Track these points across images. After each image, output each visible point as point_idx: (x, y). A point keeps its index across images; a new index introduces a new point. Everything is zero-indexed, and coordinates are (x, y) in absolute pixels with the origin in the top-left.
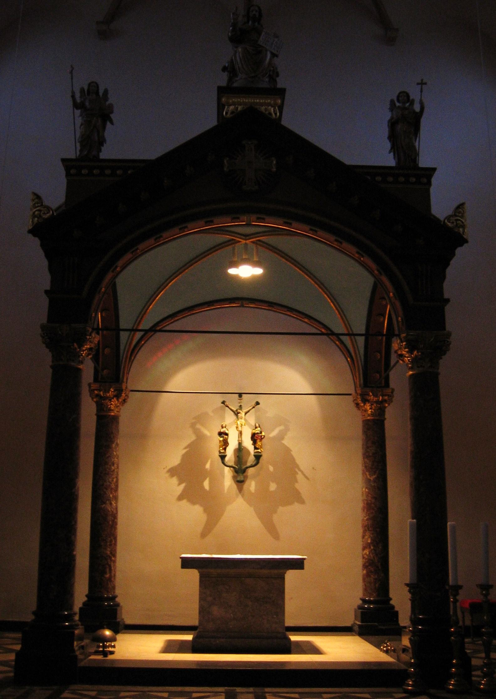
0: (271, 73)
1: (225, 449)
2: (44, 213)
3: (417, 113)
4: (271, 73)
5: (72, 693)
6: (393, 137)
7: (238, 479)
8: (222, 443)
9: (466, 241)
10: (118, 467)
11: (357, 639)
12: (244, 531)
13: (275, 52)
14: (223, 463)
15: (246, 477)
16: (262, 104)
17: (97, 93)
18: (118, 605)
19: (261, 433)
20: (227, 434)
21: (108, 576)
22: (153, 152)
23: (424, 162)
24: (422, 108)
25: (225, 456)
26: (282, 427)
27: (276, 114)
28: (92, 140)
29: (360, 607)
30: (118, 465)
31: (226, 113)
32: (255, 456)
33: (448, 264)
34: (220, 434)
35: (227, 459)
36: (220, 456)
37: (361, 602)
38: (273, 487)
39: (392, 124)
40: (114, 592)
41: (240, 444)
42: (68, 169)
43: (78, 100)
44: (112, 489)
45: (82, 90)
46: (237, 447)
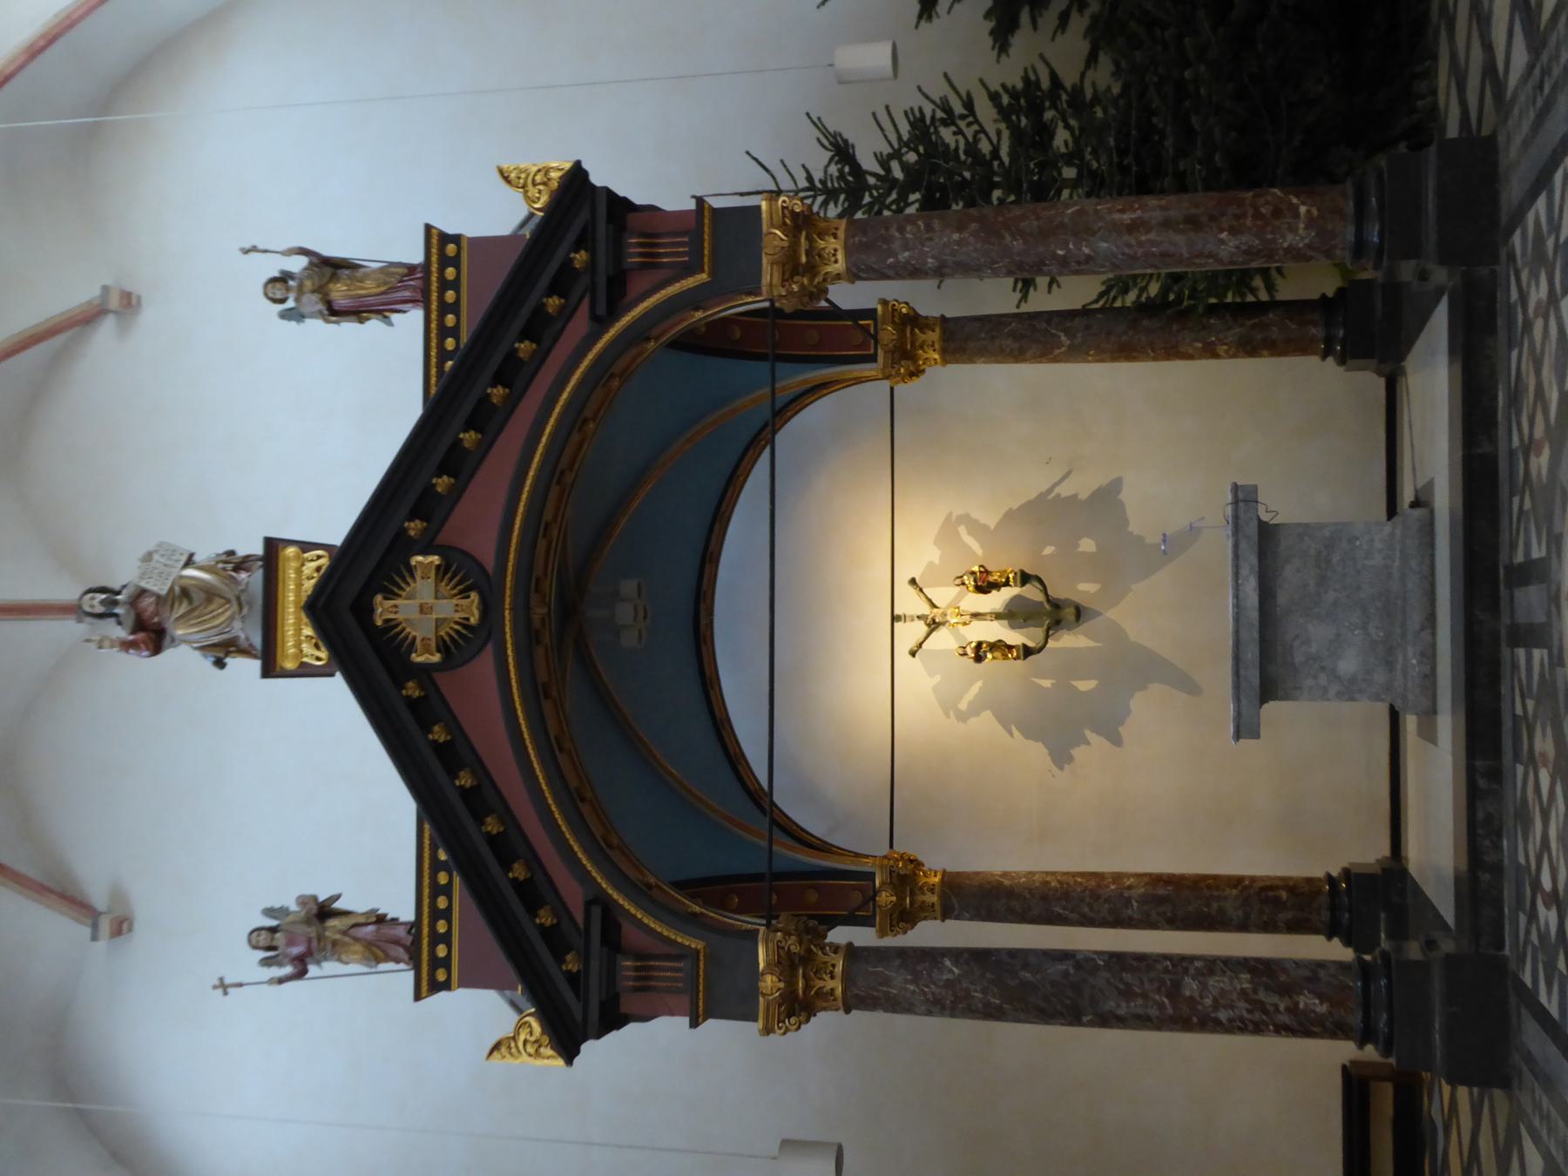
0: (230, 566)
1: (1010, 648)
2: (531, 1034)
3: (311, 263)
4: (230, 566)
5: (1524, 963)
6: (358, 313)
7: (1072, 618)
8: (998, 654)
9: (578, 165)
10: (1053, 873)
11: (1410, 363)
12: (1180, 614)
13: (184, 558)
14: (1040, 650)
15: (1068, 602)
16: (299, 585)
17: (273, 930)
18: (1347, 873)
19: (973, 573)
20: (979, 644)
21: (1284, 895)
22: (397, 806)
23: (414, 254)
24: (303, 252)
25: (1025, 646)
26: (962, 530)
27: (319, 557)
28: (376, 939)
29: (1342, 361)
30: (1047, 873)
31: (318, 659)
32: (1023, 584)
33: (625, 200)
34: (979, 658)
35: (1031, 644)
36: (1026, 656)
37: (1330, 360)
38: (1087, 545)
39: (334, 312)
40: (1319, 880)
41: (998, 616)
42: (436, 987)
43: (288, 970)
44: (1099, 886)
45: (266, 962)
46: (1005, 622)
